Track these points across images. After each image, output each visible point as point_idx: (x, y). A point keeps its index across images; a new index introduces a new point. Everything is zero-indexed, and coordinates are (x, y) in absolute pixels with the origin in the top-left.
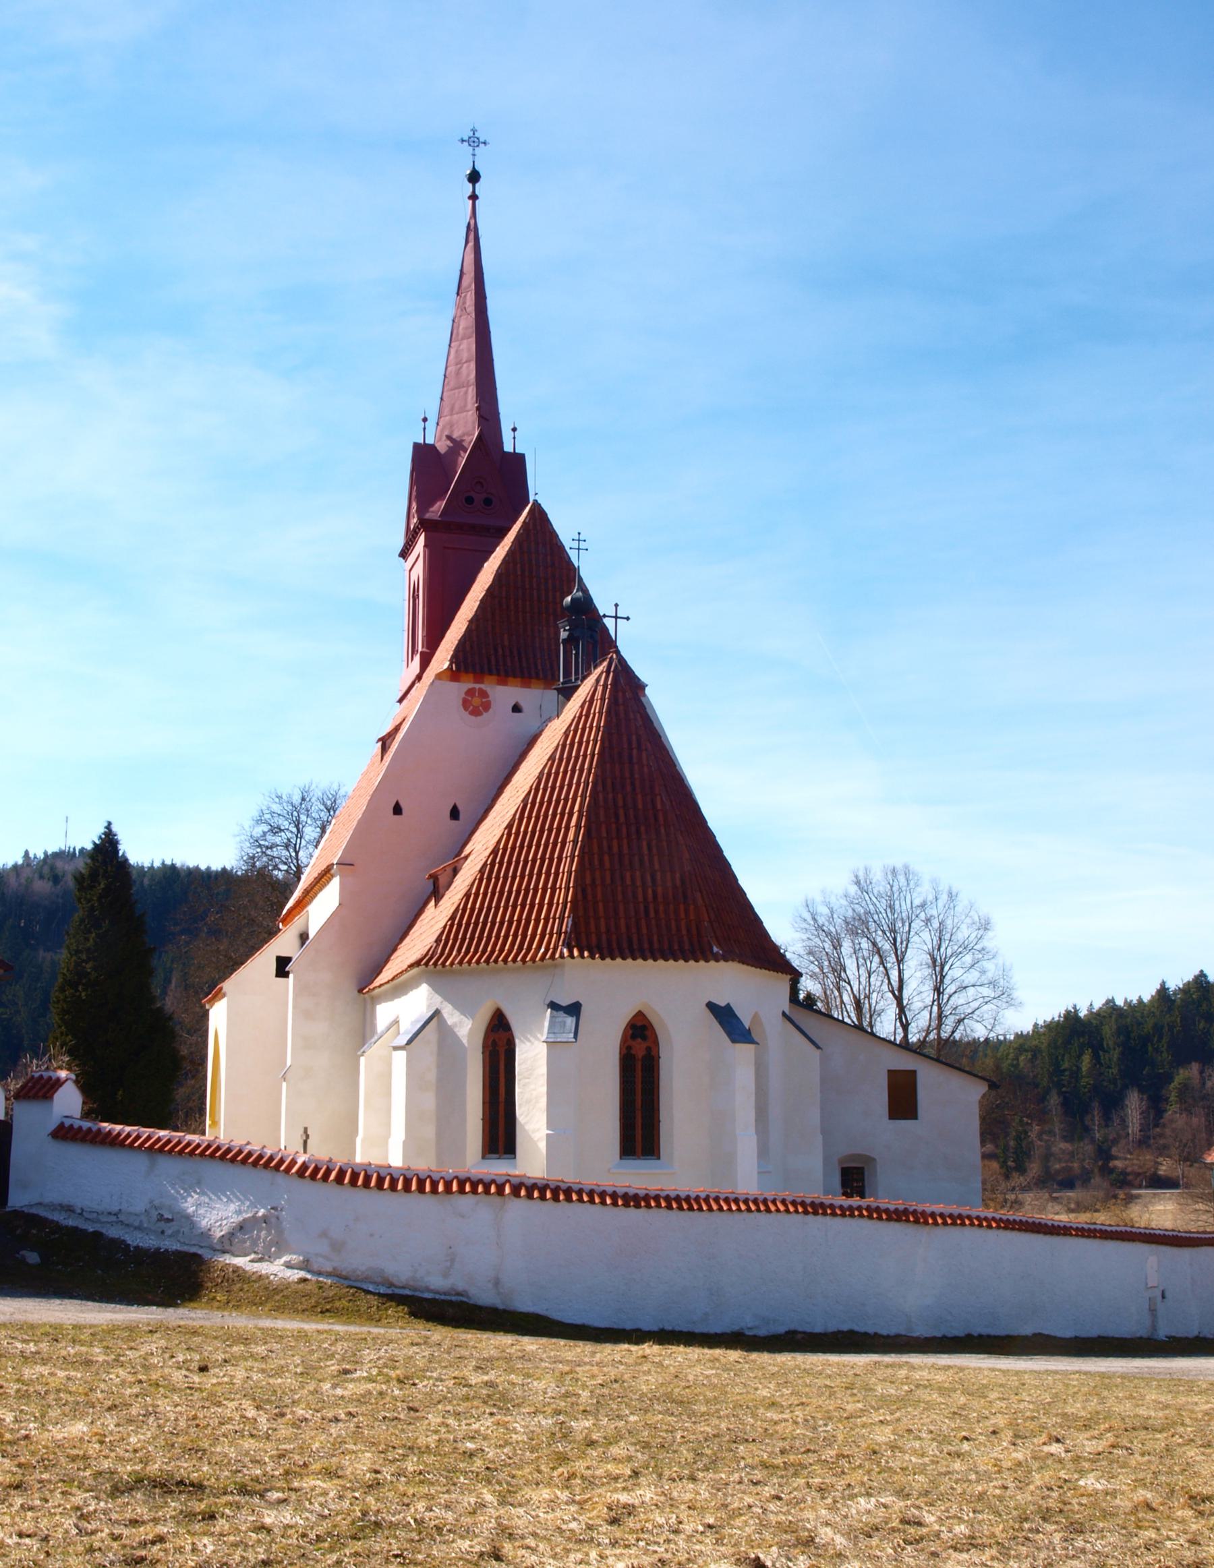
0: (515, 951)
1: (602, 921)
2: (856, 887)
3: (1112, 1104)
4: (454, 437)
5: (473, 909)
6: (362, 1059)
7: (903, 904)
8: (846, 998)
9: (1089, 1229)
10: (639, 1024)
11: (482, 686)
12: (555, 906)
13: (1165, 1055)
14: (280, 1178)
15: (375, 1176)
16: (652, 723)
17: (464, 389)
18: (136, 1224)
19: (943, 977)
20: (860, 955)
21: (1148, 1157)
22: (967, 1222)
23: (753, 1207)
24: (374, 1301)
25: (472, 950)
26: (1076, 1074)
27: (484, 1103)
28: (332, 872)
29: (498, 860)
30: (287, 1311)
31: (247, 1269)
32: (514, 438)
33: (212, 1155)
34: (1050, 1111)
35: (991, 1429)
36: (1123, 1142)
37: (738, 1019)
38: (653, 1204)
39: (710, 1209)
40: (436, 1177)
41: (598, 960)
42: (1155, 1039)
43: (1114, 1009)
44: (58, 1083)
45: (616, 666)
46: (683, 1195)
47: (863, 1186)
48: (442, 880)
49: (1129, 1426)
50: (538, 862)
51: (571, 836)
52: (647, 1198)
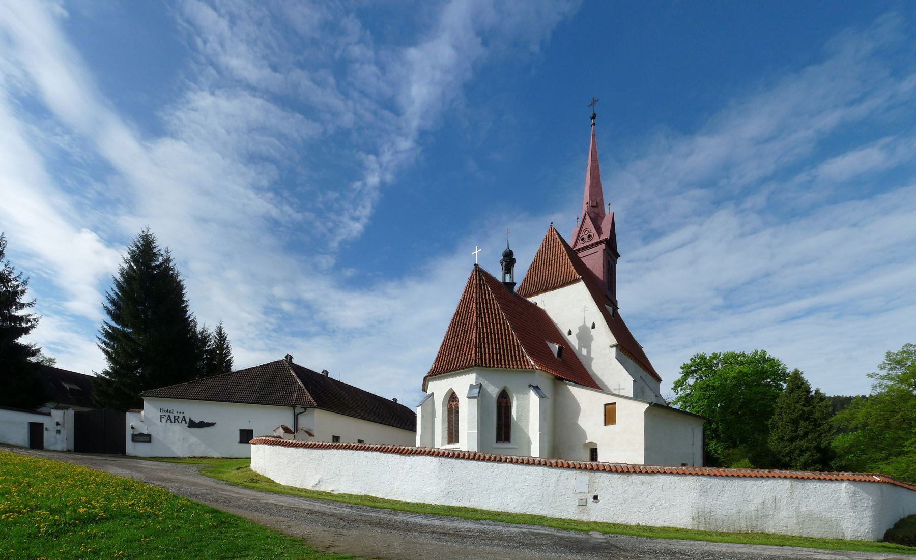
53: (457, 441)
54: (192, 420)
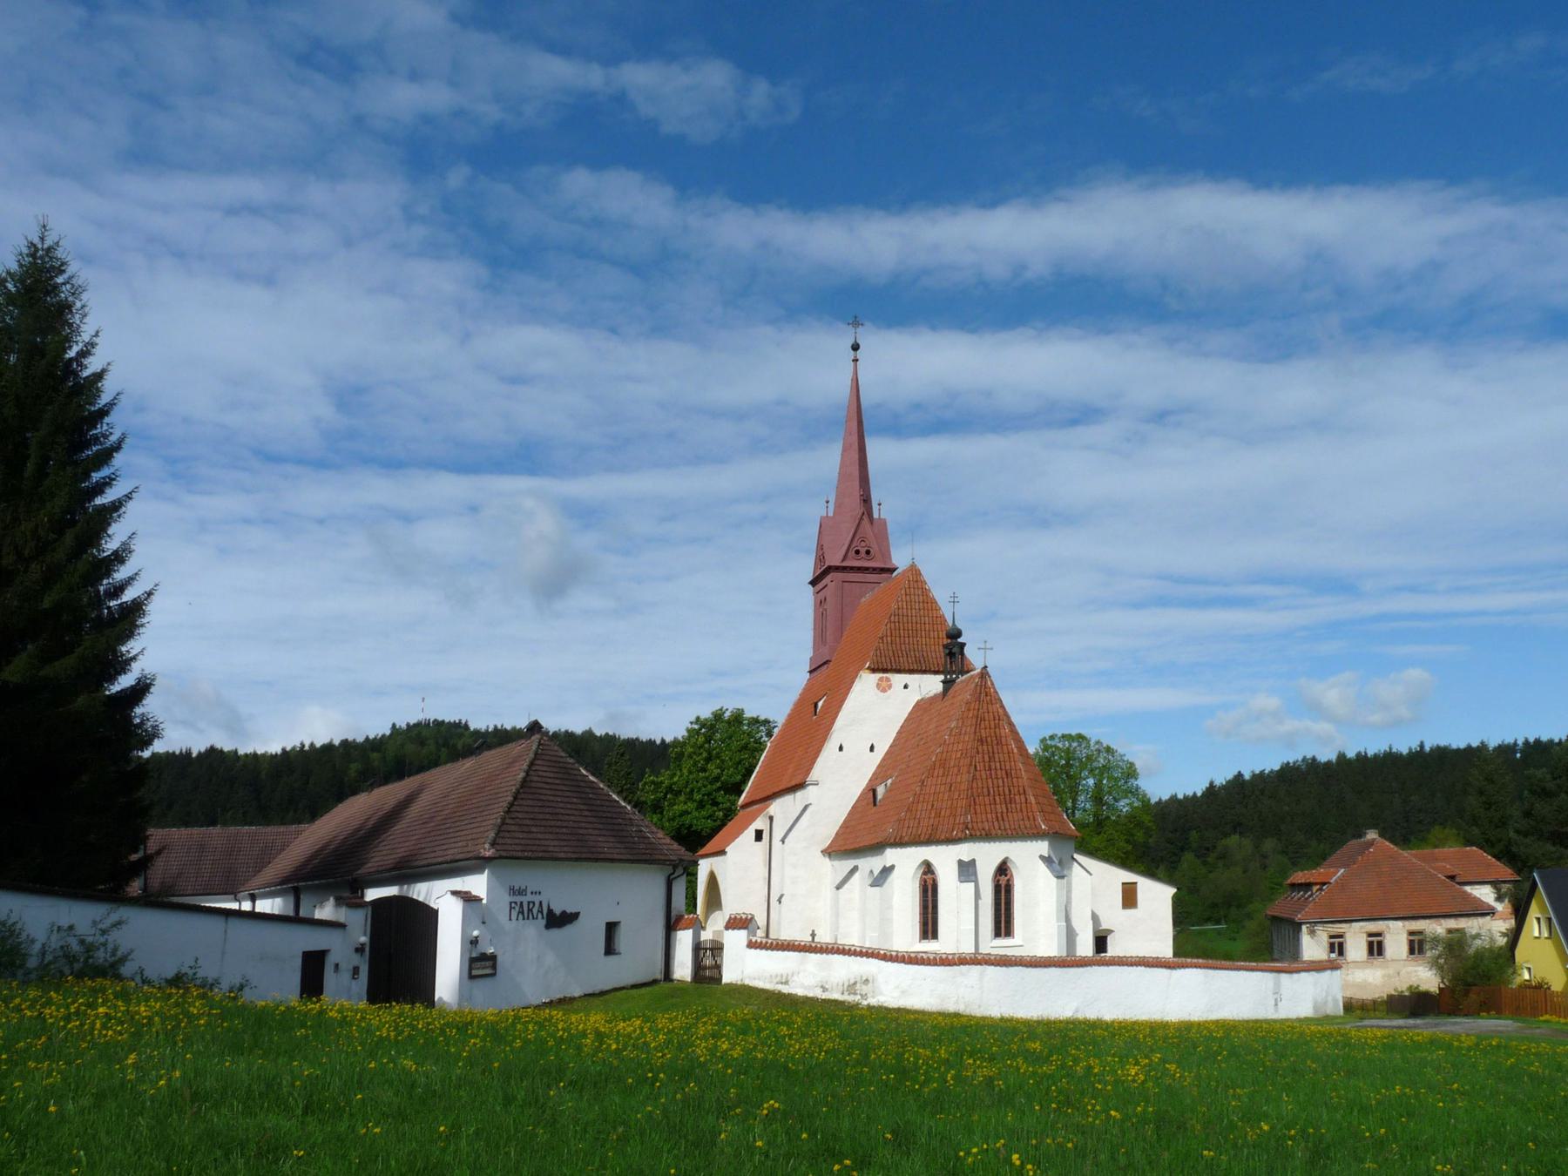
53: (935, 936)
54: (552, 910)
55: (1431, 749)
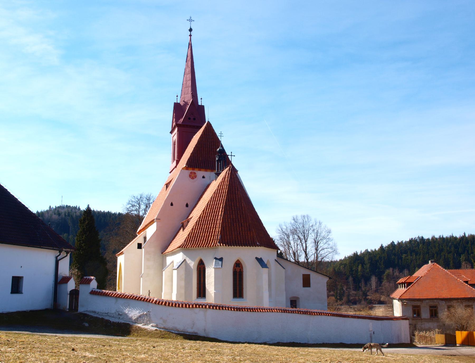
0: (205, 244)
1: (228, 236)
2: (293, 221)
3: (367, 280)
4: (185, 101)
5: (194, 233)
6: (164, 272)
7: (307, 225)
8: (291, 252)
9: (354, 316)
10: (238, 263)
11: (194, 171)
12: (216, 232)
13: (382, 265)
14: (150, 304)
15: (174, 303)
16: (241, 183)
17: (188, 88)
18: (113, 316)
19: (318, 246)
20: (295, 240)
21: (378, 295)
22: (323, 314)
23: (269, 311)
24: (174, 335)
25: (194, 243)
26: (357, 271)
27: (197, 284)
28: (154, 221)
29: (201, 220)
30: (153, 338)
31: (142, 327)
32: (201, 101)
33: (132, 298)
34: (350, 282)
35: (326, 360)
36: (371, 291)
37: (263, 261)
38: (244, 310)
39: (258, 311)
40: (189, 304)
41: (227, 246)
42: (380, 261)
43: (368, 253)
44: (91, 280)
45: (231, 169)
46: (251, 308)
47: (296, 305)
48: (185, 224)
49: (357, 359)
50: (211, 220)
51: (220, 214)
52: (242, 309)
55: (468, 236)
